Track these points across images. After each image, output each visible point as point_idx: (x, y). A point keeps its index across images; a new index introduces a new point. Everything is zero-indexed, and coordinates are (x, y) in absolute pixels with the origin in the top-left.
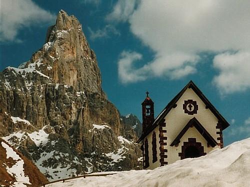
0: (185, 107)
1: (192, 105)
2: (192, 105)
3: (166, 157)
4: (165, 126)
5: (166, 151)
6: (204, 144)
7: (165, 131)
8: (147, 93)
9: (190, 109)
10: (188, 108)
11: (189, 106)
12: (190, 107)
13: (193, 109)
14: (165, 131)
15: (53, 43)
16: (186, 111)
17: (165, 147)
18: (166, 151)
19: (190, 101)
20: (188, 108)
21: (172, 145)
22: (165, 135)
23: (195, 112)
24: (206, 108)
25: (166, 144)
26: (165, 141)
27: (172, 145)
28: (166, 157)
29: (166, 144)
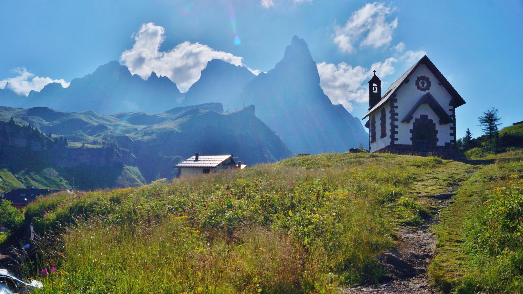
0: (417, 84)
3: (397, 133)
4: (427, 116)
5: (397, 127)
7: (397, 107)
12: (423, 83)
13: (425, 85)
14: (397, 107)
17: (396, 123)
18: (397, 127)
19: (423, 78)
20: (420, 85)
21: (403, 121)
22: (396, 111)
23: (428, 88)
25: (397, 120)
26: (396, 117)
27: (403, 121)
28: (397, 133)
29: (397, 120)
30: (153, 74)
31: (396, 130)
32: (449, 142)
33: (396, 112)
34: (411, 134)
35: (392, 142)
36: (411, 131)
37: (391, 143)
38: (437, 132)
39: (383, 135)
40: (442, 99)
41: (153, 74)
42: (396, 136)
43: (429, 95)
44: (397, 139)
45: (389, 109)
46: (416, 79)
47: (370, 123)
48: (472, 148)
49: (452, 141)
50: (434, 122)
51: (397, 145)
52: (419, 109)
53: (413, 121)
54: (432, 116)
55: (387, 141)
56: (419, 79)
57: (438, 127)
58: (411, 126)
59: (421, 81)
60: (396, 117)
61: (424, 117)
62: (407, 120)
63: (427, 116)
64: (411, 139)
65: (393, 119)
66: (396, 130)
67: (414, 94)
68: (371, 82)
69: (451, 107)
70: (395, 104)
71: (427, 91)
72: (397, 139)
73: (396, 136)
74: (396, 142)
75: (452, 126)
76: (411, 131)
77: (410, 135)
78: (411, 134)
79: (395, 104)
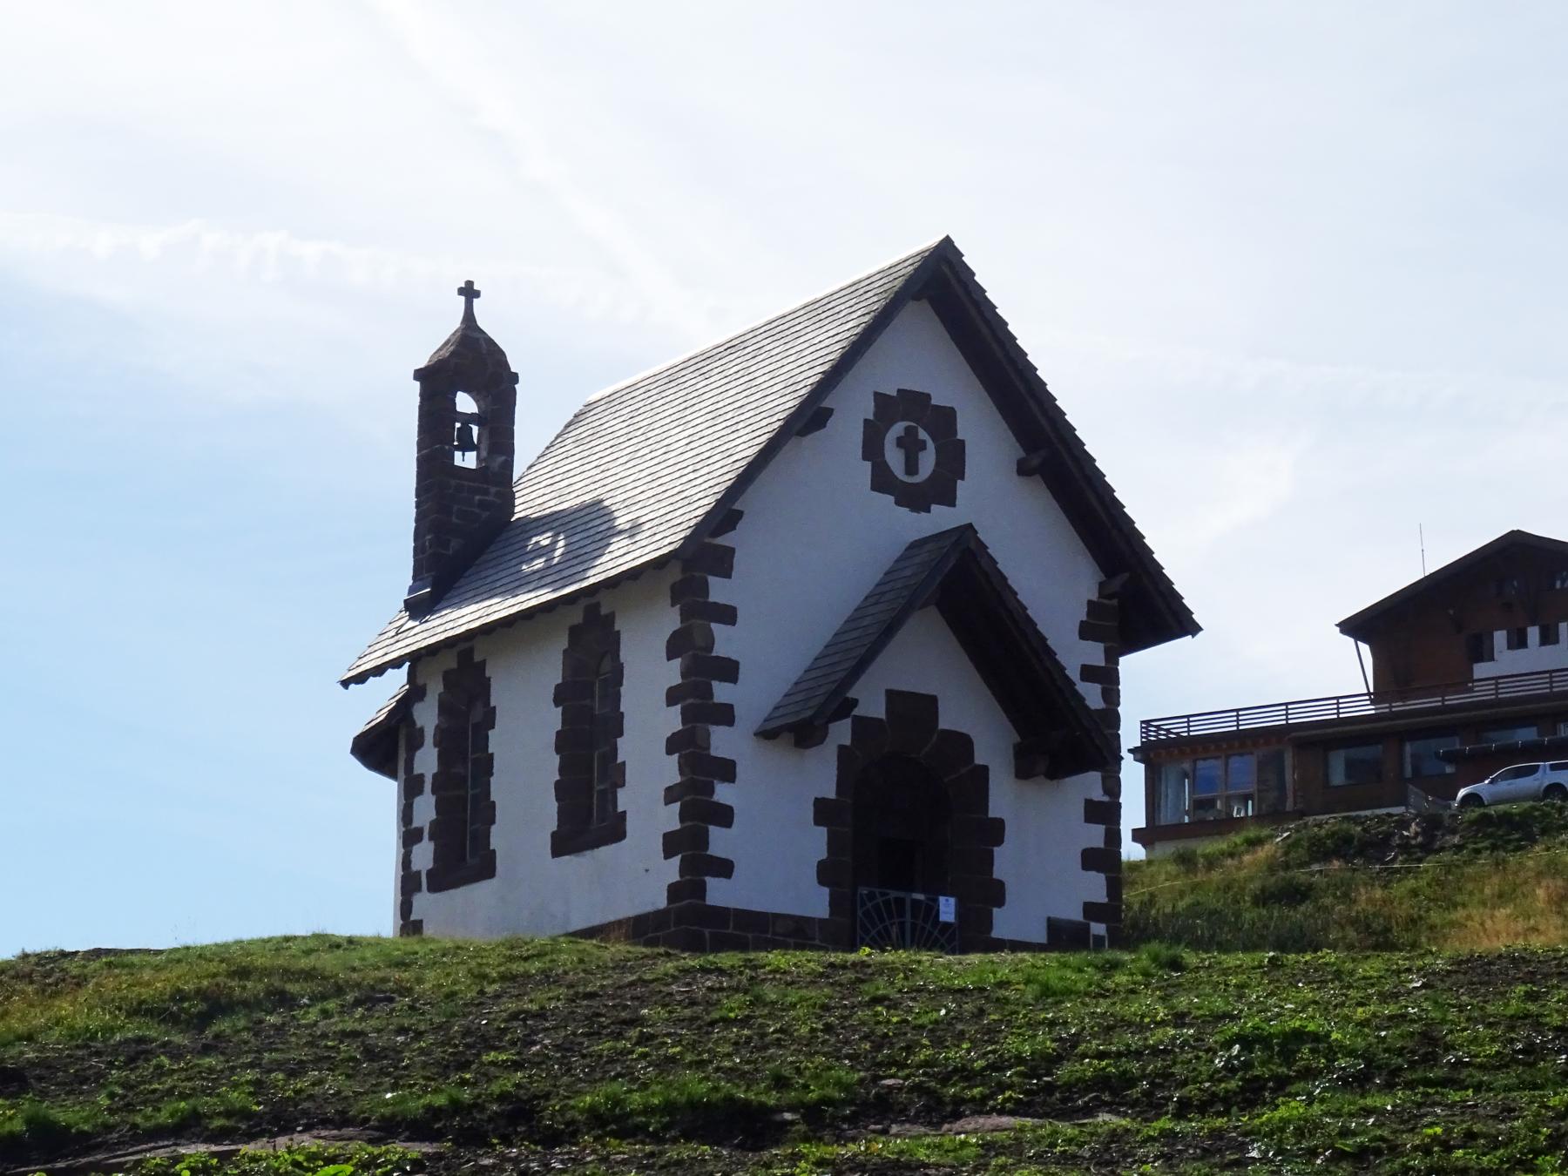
0: (872, 449)
1: (923, 435)
2: (923, 435)
3: (724, 816)
4: (932, 701)
5: (727, 771)
6: (989, 737)
7: (728, 615)
8: (469, 292)
9: (911, 468)
10: (895, 459)
11: (900, 442)
12: (910, 446)
13: (928, 462)
14: (728, 615)
15: (411, 624)
16: (882, 481)
17: (722, 742)
18: (727, 771)
19: (911, 405)
20: (895, 459)
21: (767, 734)
22: (725, 641)
23: (941, 490)
24: (1023, 470)
25: (726, 715)
26: (722, 692)
27: (767, 734)
28: (724, 816)
29: (726, 715)
30: (879, 397)
31: (723, 793)
32: (1077, 915)
33: (720, 650)
34: (822, 832)
35: (686, 891)
36: (824, 812)
37: (674, 891)
38: (995, 832)
39: (587, 819)
40: (1052, 586)
41: (879, 397)
42: (720, 842)
43: (965, 544)
44: (724, 868)
45: (670, 620)
46: (868, 410)
47: (427, 716)
48: (835, 950)
49: (1091, 910)
50: (979, 759)
51: (721, 914)
52: (901, 636)
53: (841, 733)
54: (969, 712)
55: (637, 874)
56: (888, 407)
57: (1005, 797)
58: (820, 774)
59: (898, 429)
60: (722, 692)
61: (913, 710)
62: (795, 729)
63: (932, 701)
64: (826, 872)
65: (699, 703)
66: (723, 793)
67: (850, 535)
68: (435, 382)
69: (1094, 653)
70: (719, 591)
71: (940, 519)
72: (724, 868)
73: (720, 842)
74: (719, 893)
75: (1098, 795)
76: (824, 812)
77: (815, 843)
78: (822, 832)
79: (719, 591)
